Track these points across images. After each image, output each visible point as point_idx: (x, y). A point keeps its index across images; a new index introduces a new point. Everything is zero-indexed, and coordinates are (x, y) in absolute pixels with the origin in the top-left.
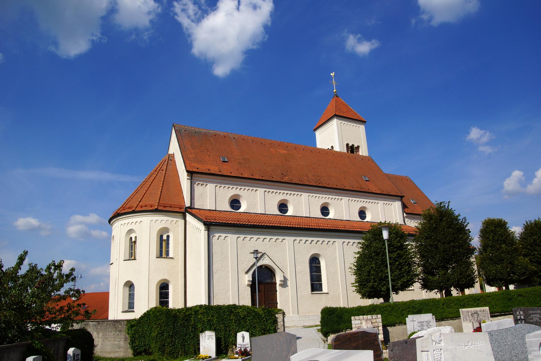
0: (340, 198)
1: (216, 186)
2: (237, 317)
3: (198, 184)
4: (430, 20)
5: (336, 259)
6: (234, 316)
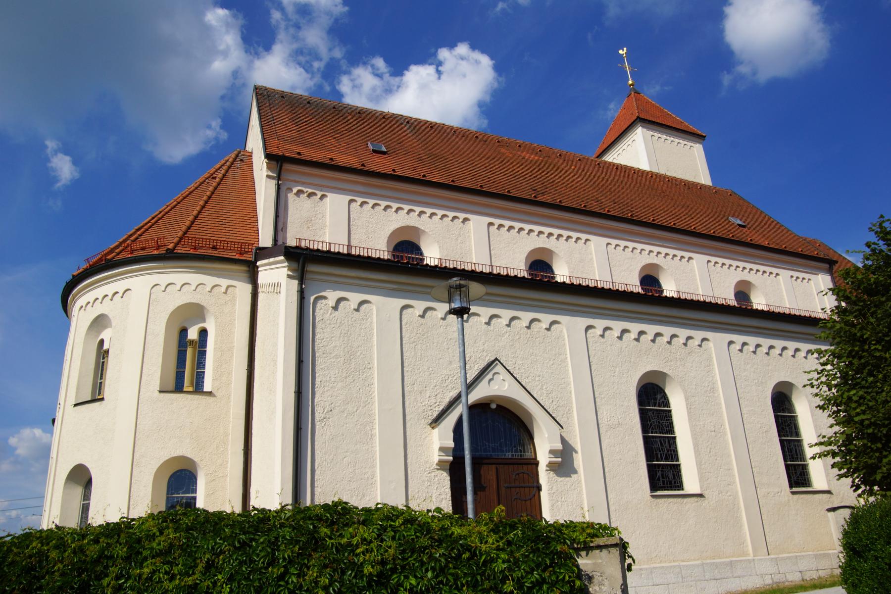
0: (687, 255)
1: (351, 201)
2: (343, 572)
3: (299, 192)
4: (754, 74)
5: (713, 390)
6: (326, 566)
